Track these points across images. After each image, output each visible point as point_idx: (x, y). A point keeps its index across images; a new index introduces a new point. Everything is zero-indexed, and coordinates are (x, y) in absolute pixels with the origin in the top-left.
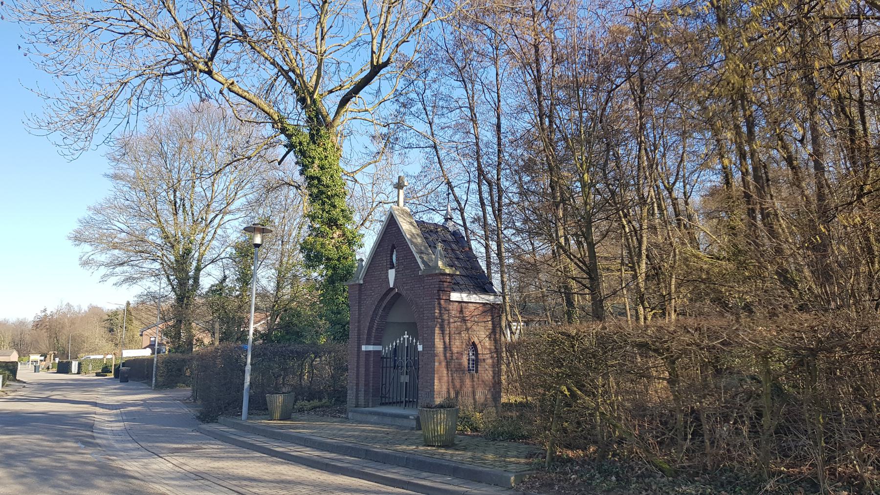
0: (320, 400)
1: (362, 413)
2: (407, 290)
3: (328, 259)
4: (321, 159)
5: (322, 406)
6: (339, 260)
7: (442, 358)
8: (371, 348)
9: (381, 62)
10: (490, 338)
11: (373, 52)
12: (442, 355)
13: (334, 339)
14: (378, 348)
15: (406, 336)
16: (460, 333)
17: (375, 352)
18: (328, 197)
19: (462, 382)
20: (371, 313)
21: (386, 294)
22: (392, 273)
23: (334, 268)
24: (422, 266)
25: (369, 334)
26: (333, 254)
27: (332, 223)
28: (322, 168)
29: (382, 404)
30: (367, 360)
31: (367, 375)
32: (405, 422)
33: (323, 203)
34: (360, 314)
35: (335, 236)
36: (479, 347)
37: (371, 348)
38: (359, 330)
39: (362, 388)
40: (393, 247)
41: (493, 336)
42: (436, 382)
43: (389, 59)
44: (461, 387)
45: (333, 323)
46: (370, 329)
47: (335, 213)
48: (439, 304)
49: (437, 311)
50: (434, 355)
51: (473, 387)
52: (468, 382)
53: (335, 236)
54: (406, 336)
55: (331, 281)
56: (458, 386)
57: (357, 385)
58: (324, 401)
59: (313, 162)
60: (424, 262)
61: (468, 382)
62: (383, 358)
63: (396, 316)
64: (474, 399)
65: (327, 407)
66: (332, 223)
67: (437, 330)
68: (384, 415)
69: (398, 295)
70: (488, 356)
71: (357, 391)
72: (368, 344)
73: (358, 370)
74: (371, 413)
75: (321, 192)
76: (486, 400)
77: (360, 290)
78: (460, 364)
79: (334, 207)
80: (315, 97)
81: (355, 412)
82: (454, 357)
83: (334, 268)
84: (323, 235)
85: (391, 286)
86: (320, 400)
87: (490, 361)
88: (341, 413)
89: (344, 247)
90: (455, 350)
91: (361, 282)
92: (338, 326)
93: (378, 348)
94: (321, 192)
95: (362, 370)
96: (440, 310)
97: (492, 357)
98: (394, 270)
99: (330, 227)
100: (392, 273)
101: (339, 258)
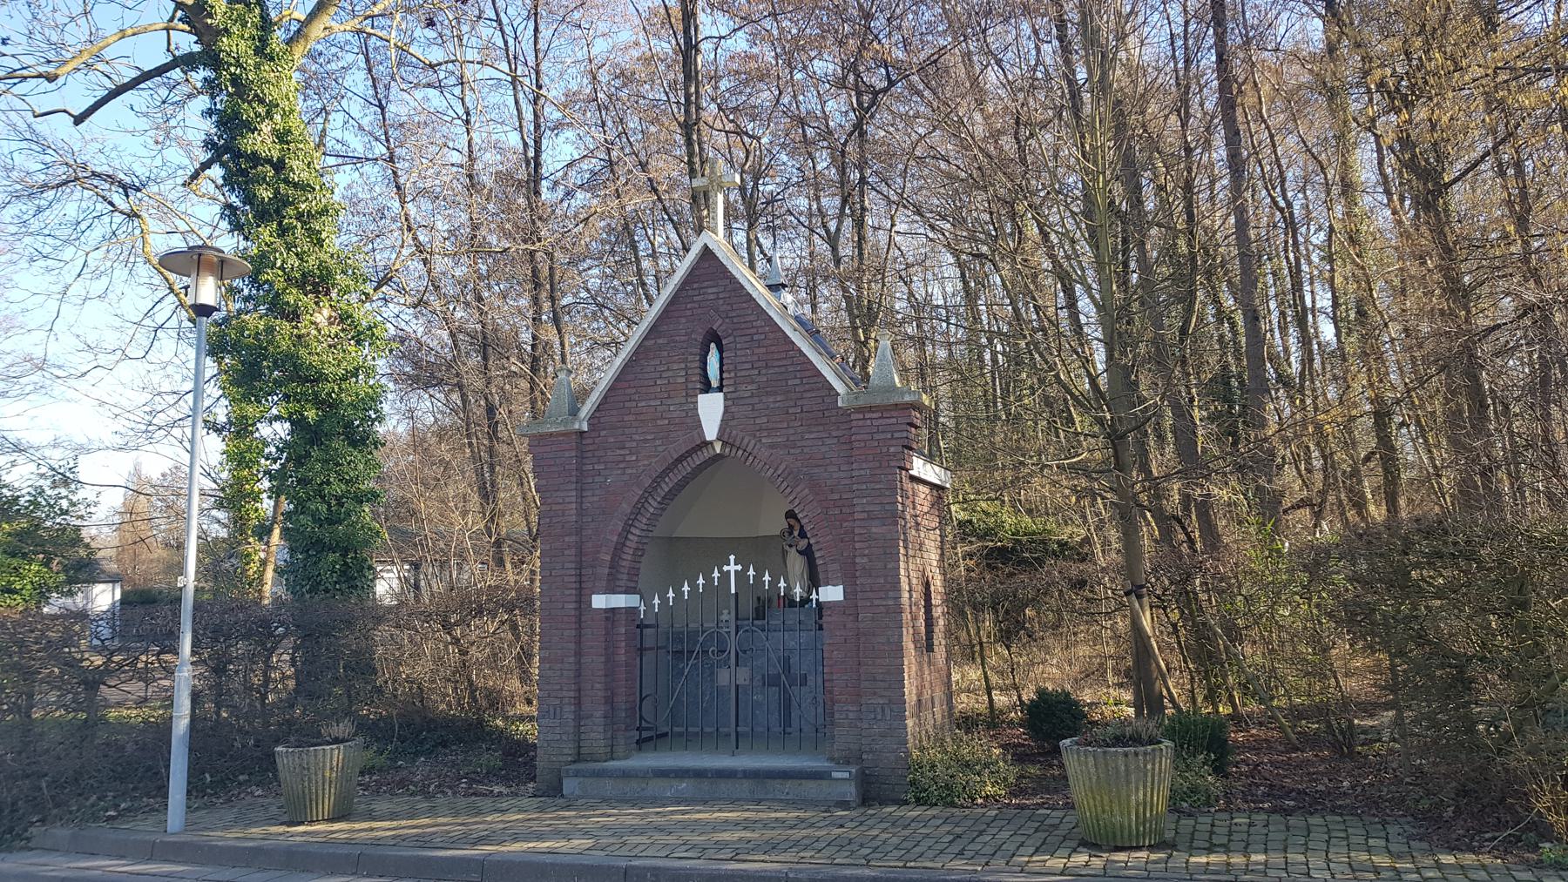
2: (772, 446)
8: (620, 601)
15: (732, 568)
20: (626, 508)
22: (711, 410)
37: (620, 601)
54: (732, 568)
91: (585, 427)
100: (711, 410)
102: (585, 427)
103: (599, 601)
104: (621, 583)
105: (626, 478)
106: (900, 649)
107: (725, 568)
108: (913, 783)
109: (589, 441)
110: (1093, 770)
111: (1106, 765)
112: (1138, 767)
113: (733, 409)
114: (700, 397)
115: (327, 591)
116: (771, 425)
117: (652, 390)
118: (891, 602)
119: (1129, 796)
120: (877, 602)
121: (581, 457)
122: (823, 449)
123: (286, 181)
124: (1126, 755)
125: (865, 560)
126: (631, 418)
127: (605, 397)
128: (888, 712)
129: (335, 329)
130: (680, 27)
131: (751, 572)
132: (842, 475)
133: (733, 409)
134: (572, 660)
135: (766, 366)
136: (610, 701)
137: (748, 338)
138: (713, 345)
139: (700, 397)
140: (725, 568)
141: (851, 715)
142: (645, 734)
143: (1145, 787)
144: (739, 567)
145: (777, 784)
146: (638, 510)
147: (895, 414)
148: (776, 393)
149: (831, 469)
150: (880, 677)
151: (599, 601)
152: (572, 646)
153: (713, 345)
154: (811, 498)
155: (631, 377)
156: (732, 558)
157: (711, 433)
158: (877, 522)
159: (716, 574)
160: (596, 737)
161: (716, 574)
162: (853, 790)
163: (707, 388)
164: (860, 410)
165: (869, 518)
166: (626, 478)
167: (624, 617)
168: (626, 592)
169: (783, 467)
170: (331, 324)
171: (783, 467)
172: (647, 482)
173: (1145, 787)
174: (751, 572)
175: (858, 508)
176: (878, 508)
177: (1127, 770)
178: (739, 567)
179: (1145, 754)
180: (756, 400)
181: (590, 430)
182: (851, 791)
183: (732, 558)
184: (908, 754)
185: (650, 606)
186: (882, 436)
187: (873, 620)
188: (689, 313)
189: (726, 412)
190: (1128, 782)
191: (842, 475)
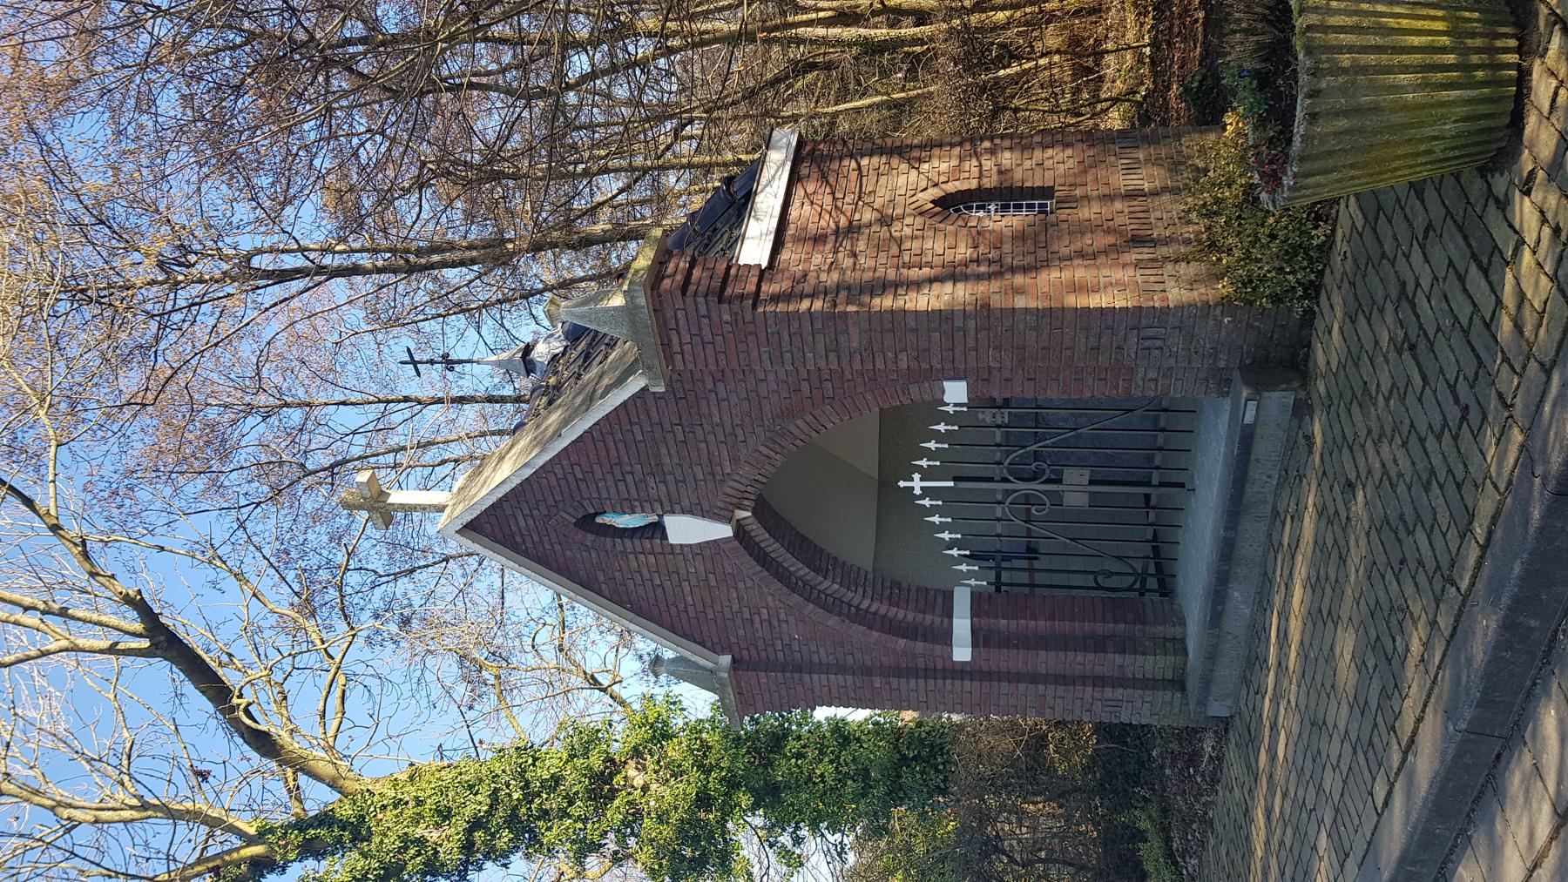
0: (1140, 836)
1: (1212, 655)
2: (735, 460)
3: (703, 800)
4: (417, 820)
5: (1165, 830)
6: (706, 770)
7: (995, 285)
8: (962, 626)
9: (138, 627)
10: (920, 160)
11: (112, 650)
12: (982, 288)
13: (944, 792)
14: (962, 600)
15: (917, 484)
16: (900, 242)
17: (975, 613)
18: (529, 797)
19: (1083, 229)
20: (833, 621)
21: (762, 558)
22: (685, 530)
23: (732, 784)
24: (635, 384)
25: (911, 632)
26: (687, 787)
27: (602, 787)
28: (444, 815)
29: (1166, 588)
30: (1008, 641)
31: (1061, 643)
32: (1267, 449)
33: (545, 814)
34: (841, 669)
35: (639, 781)
36: (952, 187)
37: (962, 626)
38: (898, 672)
39: (1113, 662)
40: (587, 523)
41: (915, 153)
42: (1095, 301)
43: (128, 600)
44: (1109, 231)
45: (896, 794)
46: (893, 628)
47: (573, 781)
48: (776, 298)
49: (805, 304)
50: (984, 310)
51: (1108, 198)
52: (1087, 212)
53: (639, 781)
54: (917, 484)
55: (768, 796)
56: (1110, 239)
57: (1100, 681)
58: (1144, 824)
59: (421, 842)
60: (620, 382)
61: (1087, 212)
62: (998, 584)
63: (852, 536)
64: (1154, 193)
65: (1165, 811)
66: (602, 787)
67: (887, 302)
68: (1227, 551)
69: (762, 510)
70: (988, 164)
71: (1121, 682)
72: (946, 637)
73: (1046, 679)
74: (1216, 617)
75: (512, 820)
76: (1157, 162)
77: (753, 667)
78: (1020, 237)
79: (557, 780)
80: (252, 831)
81: (1206, 683)
82: (993, 255)
83: (732, 784)
84: (634, 816)
85: (724, 531)
86: (1140, 836)
87: (1006, 158)
88: (1194, 758)
89: (674, 751)
90: (964, 251)
91: (726, 660)
92: (906, 780)
93: (962, 600)
94: (512, 820)
95: (1045, 661)
96: (802, 297)
97: (993, 152)
98: (670, 522)
99: (613, 793)
100: (685, 530)
101: (701, 767)
102: (726, 660)
103: (962, 653)
104: (938, 620)
105: (792, 619)
106: (1052, 317)
107: (918, 492)
108: (1276, 299)
109: (745, 653)
110: (1335, 176)
111: (1329, 153)
112: (1344, 90)
113: (686, 504)
114: (671, 541)
115: (945, 780)
116: (705, 461)
117: (669, 590)
118: (972, 324)
119: (1406, 107)
120: (971, 343)
121: (769, 666)
122: (734, 399)
123: (489, 813)
124: (1313, 117)
125: (903, 356)
126: (710, 612)
127: (685, 636)
128: (1152, 332)
129: (650, 764)
130: (296, 285)
131: (924, 463)
132: (771, 377)
133: (686, 504)
134: (1041, 687)
135: (620, 464)
136: (1099, 645)
137: (582, 485)
138: (599, 520)
139: (671, 541)
140: (918, 492)
141: (1152, 374)
142: (1152, 583)
143: (1389, 70)
144: (917, 476)
145: (1250, 490)
146: (833, 605)
147: (669, 314)
148: (658, 456)
149: (763, 392)
150: (1093, 342)
151: (962, 653)
152: (1022, 687)
153: (599, 520)
154: (809, 418)
155: (656, 612)
156: (902, 484)
157: (724, 531)
158: (843, 339)
159: (927, 502)
160: (1153, 664)
161: (927, 502)
162: (1276, 395)
163: (658, 529)
164: (669, 359)
165: (837, 351)
166: (792, 619)
167: (984, 621)
168: (950, 617)
169: (765, 450)
170: (644, 768)
171: (765, 450)
172: (796, 598)
173: (1389, 70)
174: (924, 463)
175: (822, 364)
176: (820, 338)
177: (1347, 113)
178: (917, 476)
179: (1315, 73)
180: (670, 478)
181: (731, 652)
182: (1279, 400)
183: (902, 484)
184: (1225, 303)
185: (969, 575)
186: (706, 332)
187: (998, 348)
188: (557, 547)
189: (691, 512)
190: (1375, 109)
191: (771, 377)
